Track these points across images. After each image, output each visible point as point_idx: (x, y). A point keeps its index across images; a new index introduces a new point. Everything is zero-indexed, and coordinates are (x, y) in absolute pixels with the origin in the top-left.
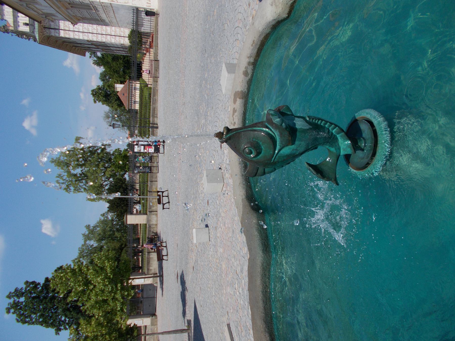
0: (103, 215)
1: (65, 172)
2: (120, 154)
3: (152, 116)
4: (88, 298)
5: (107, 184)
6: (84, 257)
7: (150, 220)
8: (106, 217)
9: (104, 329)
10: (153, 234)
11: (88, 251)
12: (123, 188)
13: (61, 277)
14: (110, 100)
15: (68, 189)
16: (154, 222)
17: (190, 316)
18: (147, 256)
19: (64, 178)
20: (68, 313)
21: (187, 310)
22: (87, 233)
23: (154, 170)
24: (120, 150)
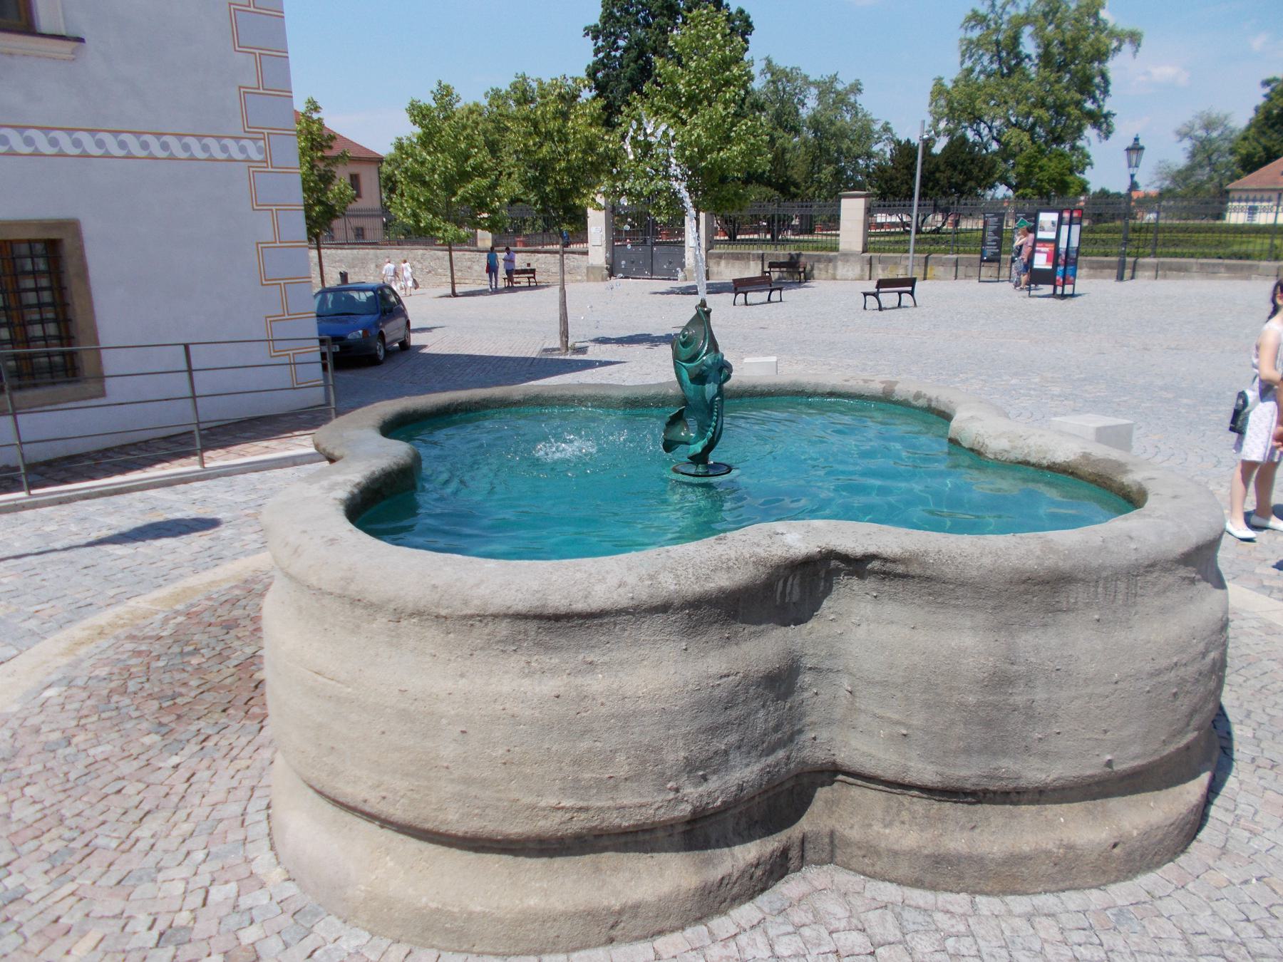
0: (886, 128)
1: (1027, 8)
2: (1071, 171)
3: (1162, 263)
4: (659, 108)
5: (980, 134)
6: (774, 82)
7: (847, 261)
8: (880, 137)
9: (580, 155)
10: (808, 268)
11: (790, 94)
12: (964, 184)
13: (714, 36)
14: (1269, 132)
15: (973, 23)
16: (843, 270)
17: (595, 353)
18: (755, 252)
19: (1008, 8)
20: (633, 54)
21: (608, 346)
22: (840, 87)
23: (987, 271)
24: (1084, 169)
